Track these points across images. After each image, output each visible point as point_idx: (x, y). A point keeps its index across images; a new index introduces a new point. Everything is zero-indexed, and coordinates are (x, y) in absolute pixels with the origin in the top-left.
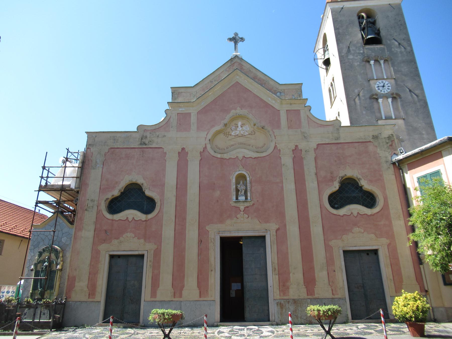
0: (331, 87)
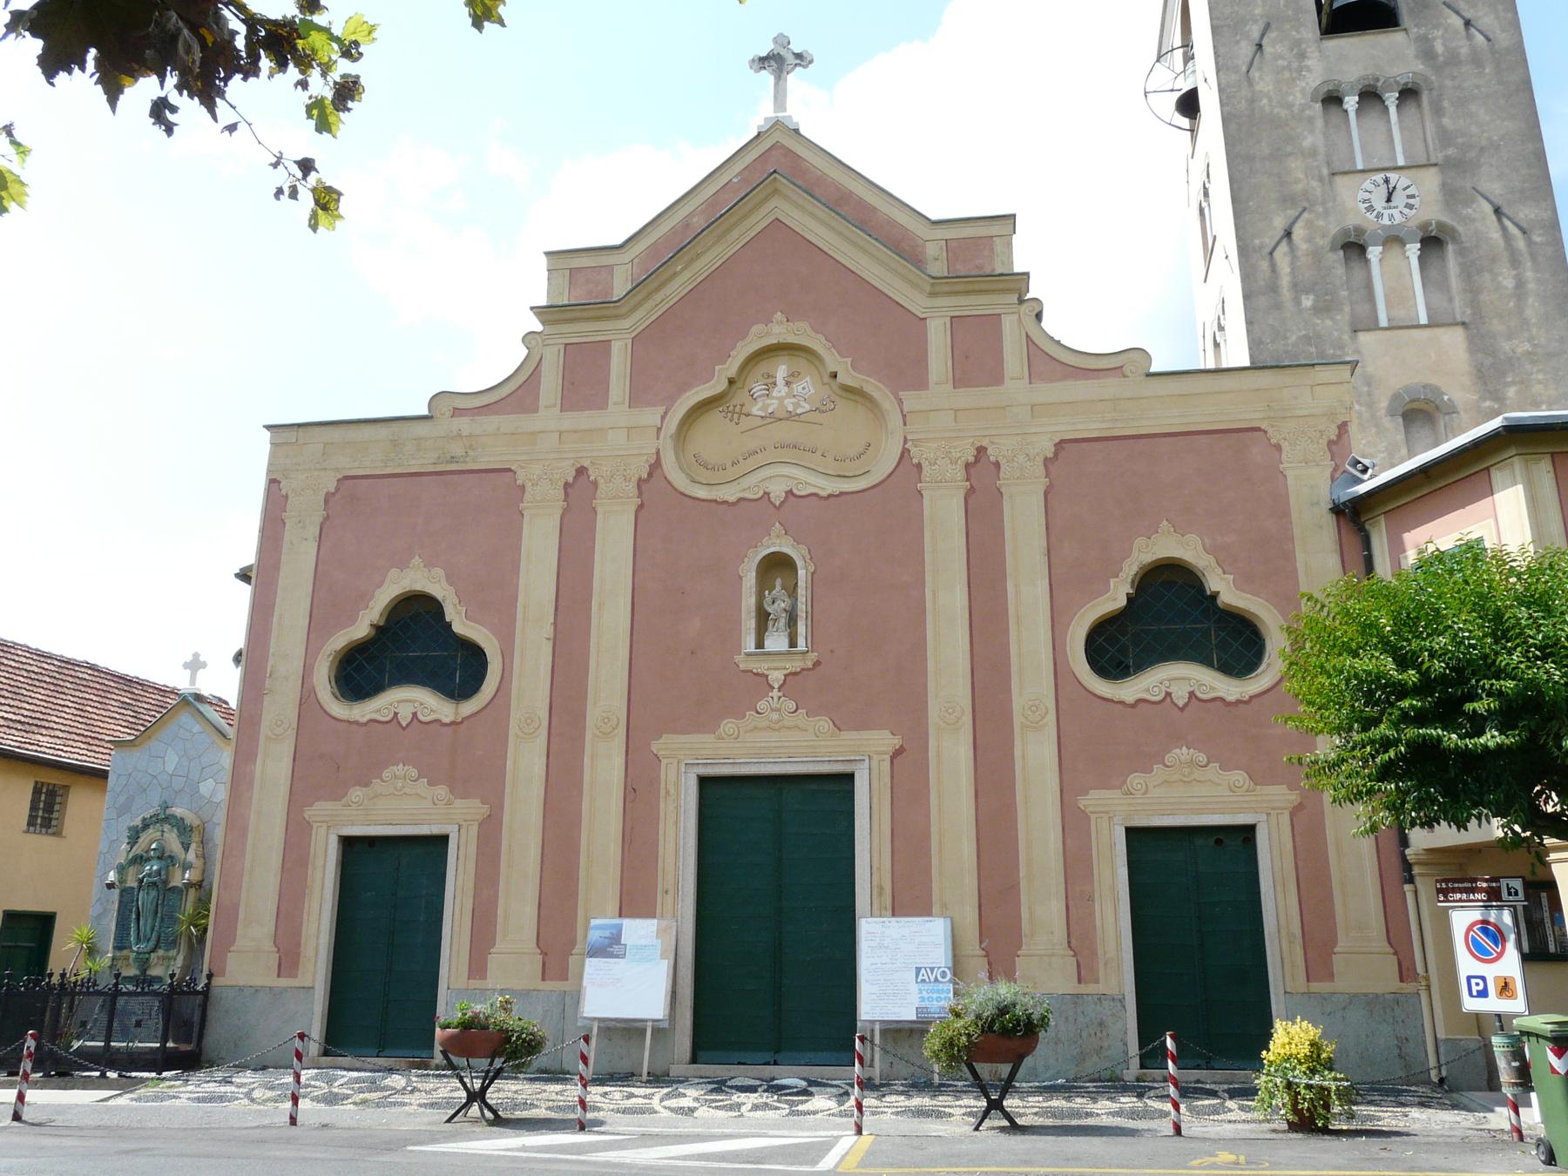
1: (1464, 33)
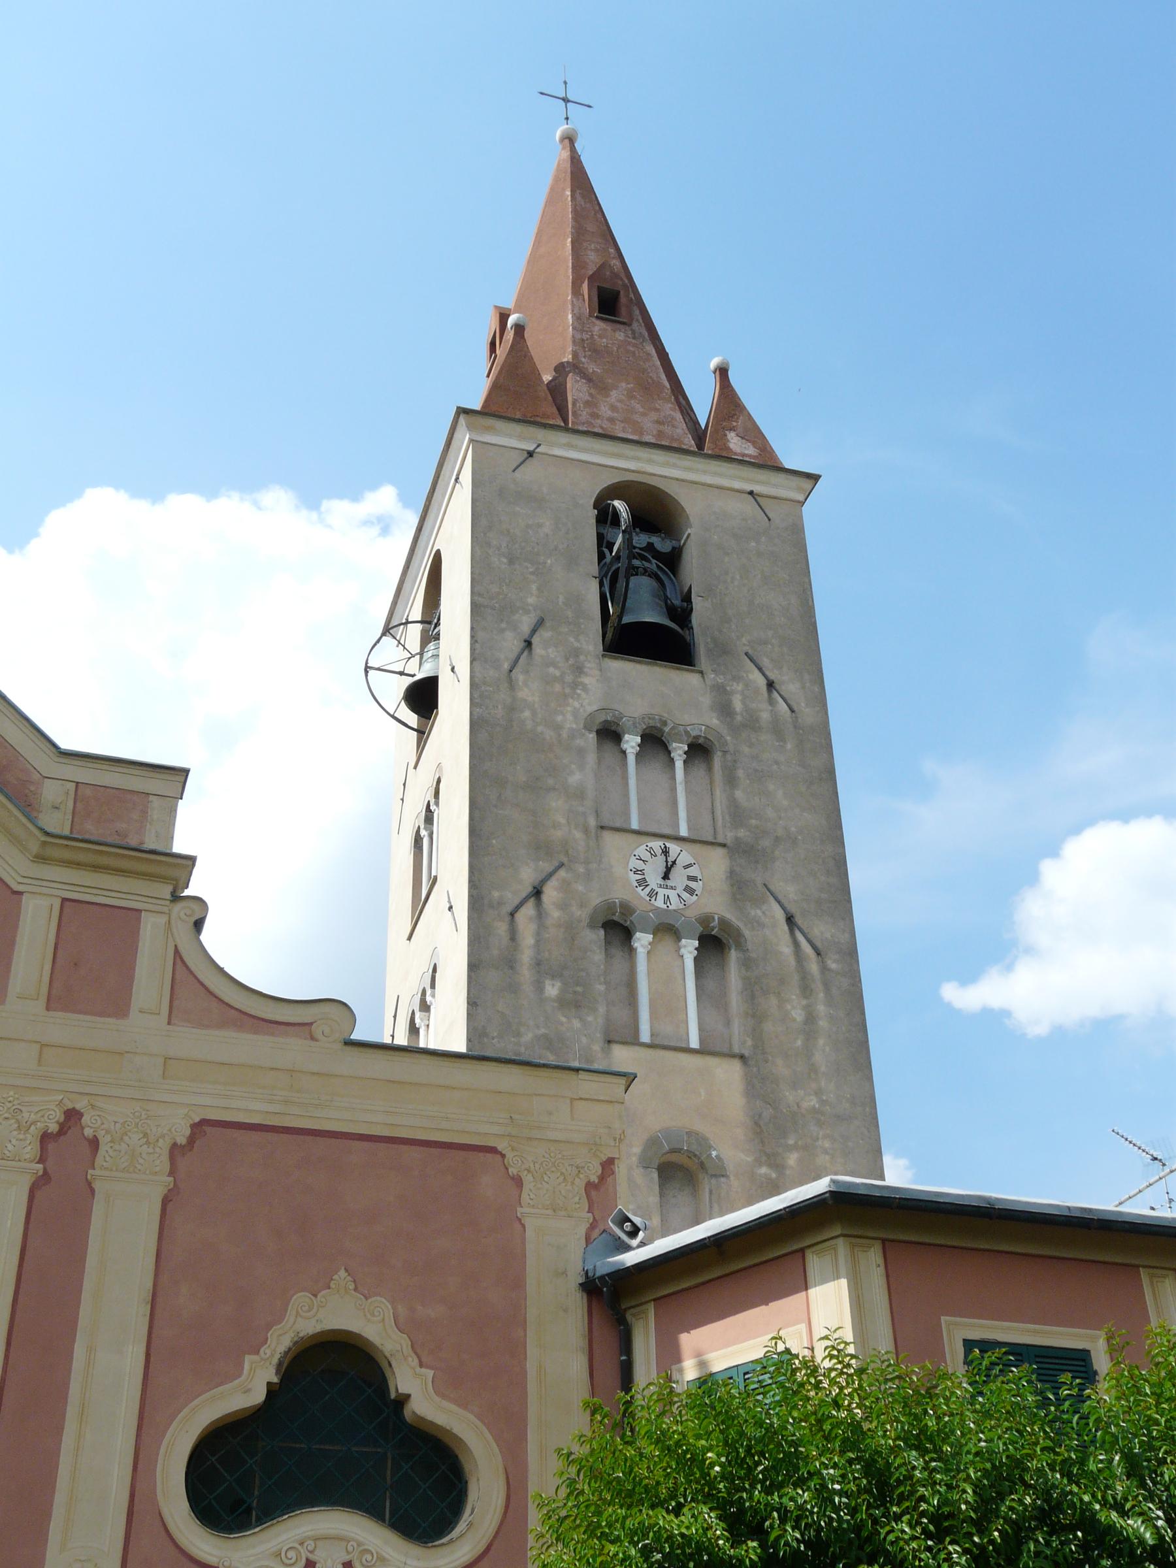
0: (425, 829)
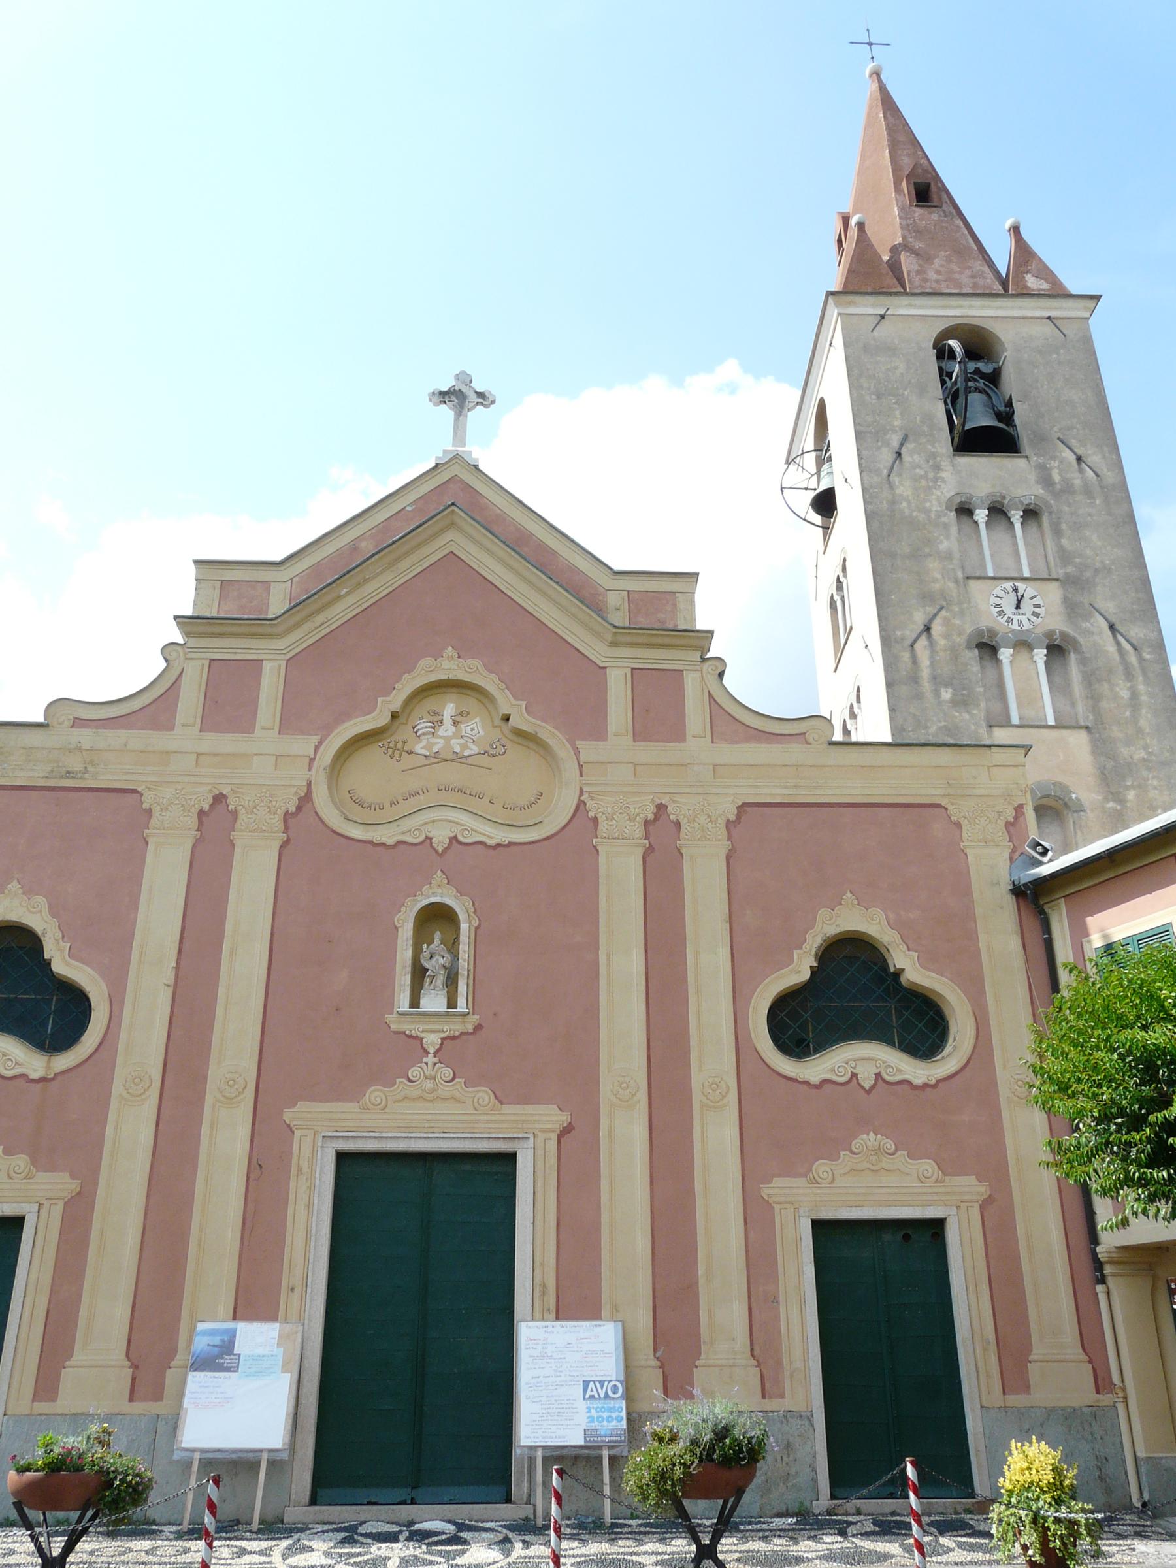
0: (837, 595)
1: (1076, 467)
